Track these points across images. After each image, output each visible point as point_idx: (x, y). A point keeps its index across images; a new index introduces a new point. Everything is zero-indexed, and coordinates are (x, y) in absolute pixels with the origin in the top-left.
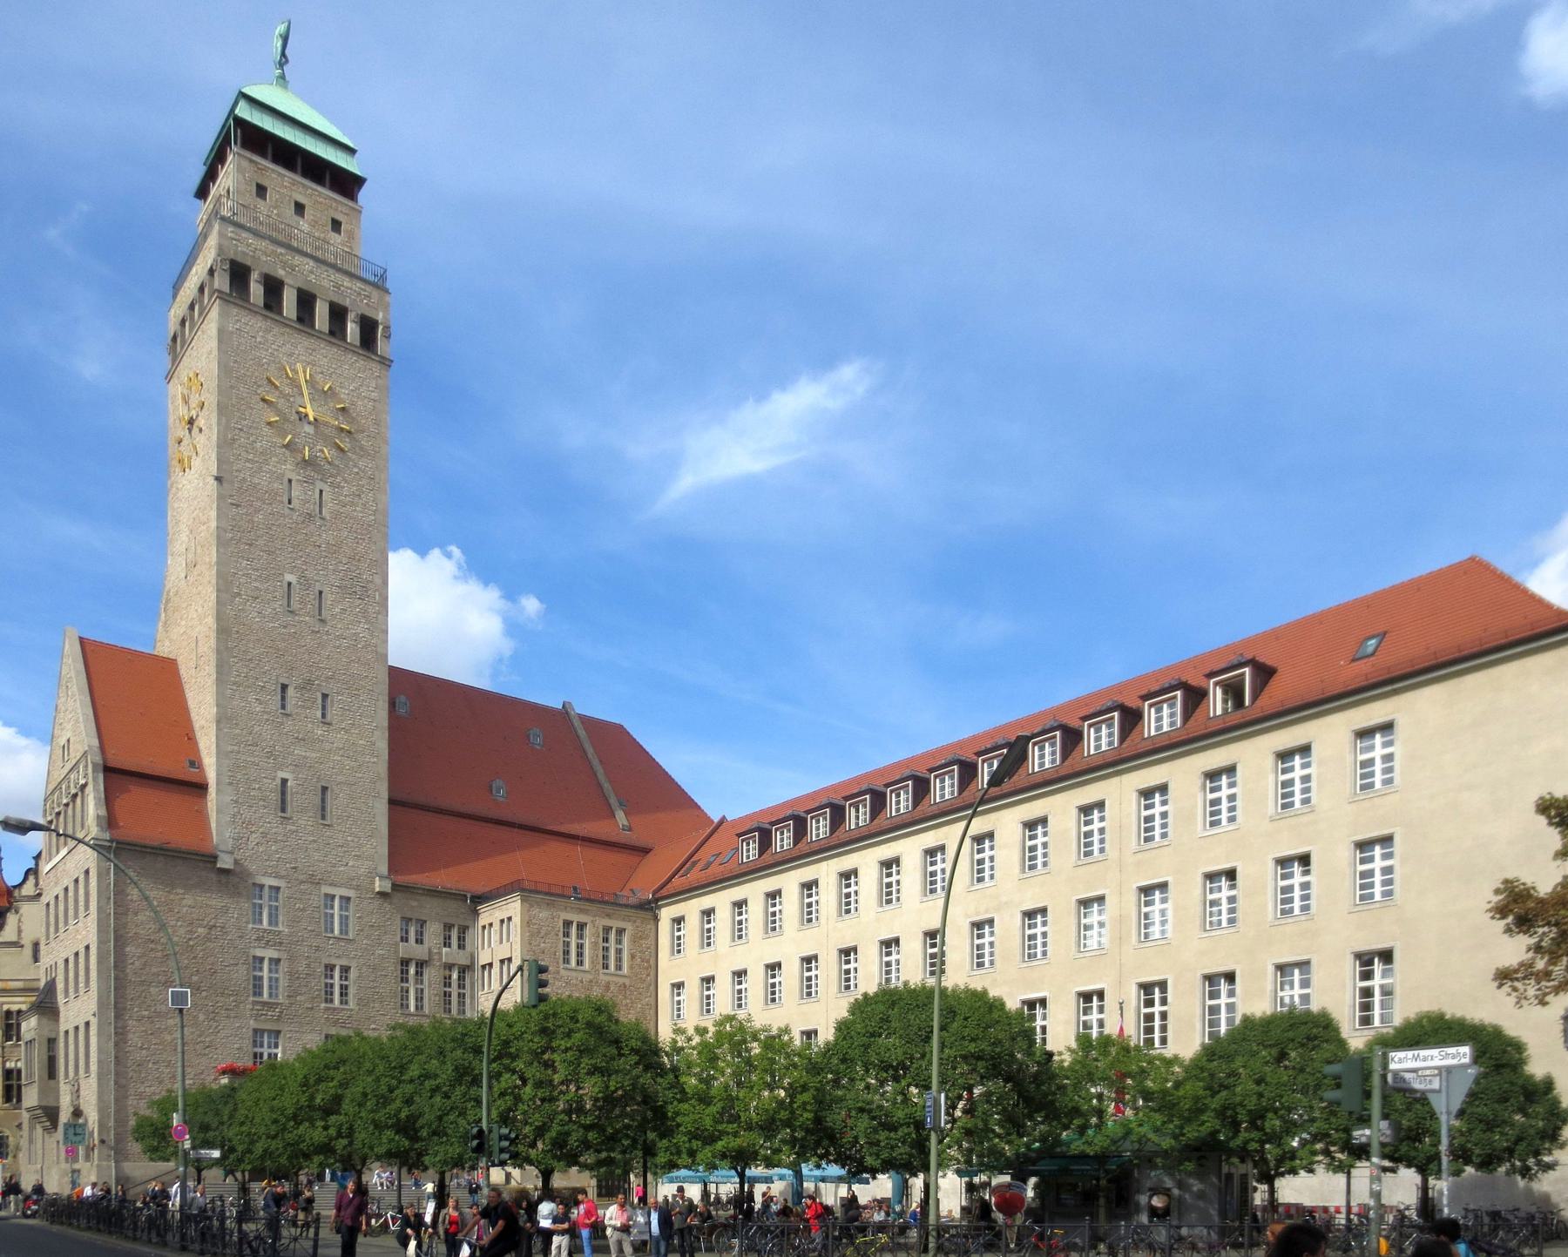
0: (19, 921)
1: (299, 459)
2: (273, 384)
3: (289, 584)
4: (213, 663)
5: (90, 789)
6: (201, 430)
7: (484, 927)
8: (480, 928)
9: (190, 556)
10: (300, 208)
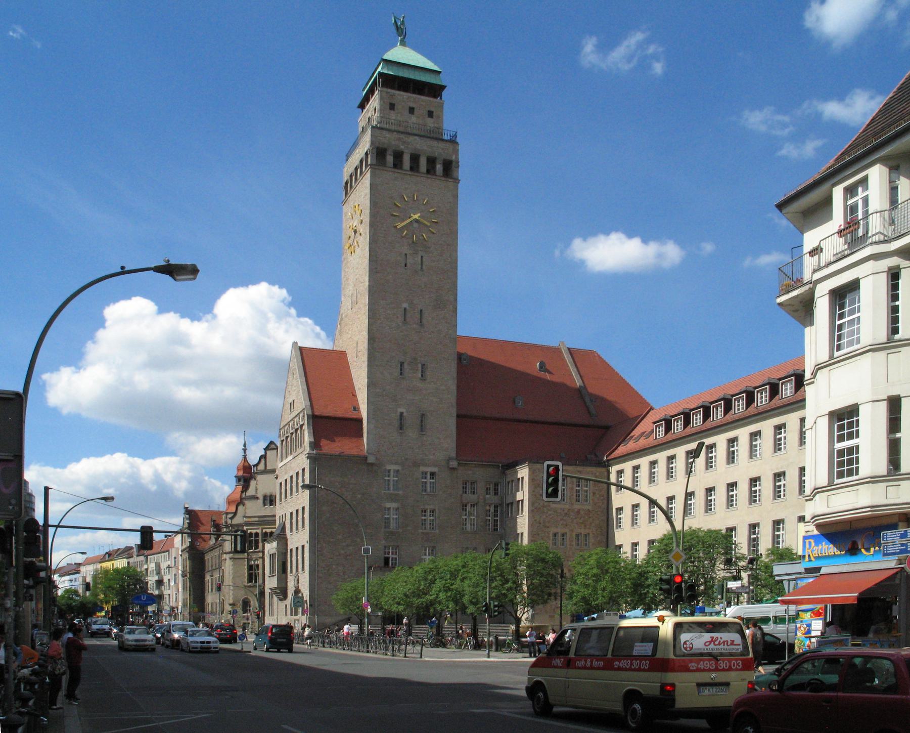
0: (257, 484)
1: (411, 242)
2: (397, 206)
3: (405, 309)
4: (366, 356)
5: (305, 427)
6: (360, 234)
7: (509, 482)
9: (354, 298)
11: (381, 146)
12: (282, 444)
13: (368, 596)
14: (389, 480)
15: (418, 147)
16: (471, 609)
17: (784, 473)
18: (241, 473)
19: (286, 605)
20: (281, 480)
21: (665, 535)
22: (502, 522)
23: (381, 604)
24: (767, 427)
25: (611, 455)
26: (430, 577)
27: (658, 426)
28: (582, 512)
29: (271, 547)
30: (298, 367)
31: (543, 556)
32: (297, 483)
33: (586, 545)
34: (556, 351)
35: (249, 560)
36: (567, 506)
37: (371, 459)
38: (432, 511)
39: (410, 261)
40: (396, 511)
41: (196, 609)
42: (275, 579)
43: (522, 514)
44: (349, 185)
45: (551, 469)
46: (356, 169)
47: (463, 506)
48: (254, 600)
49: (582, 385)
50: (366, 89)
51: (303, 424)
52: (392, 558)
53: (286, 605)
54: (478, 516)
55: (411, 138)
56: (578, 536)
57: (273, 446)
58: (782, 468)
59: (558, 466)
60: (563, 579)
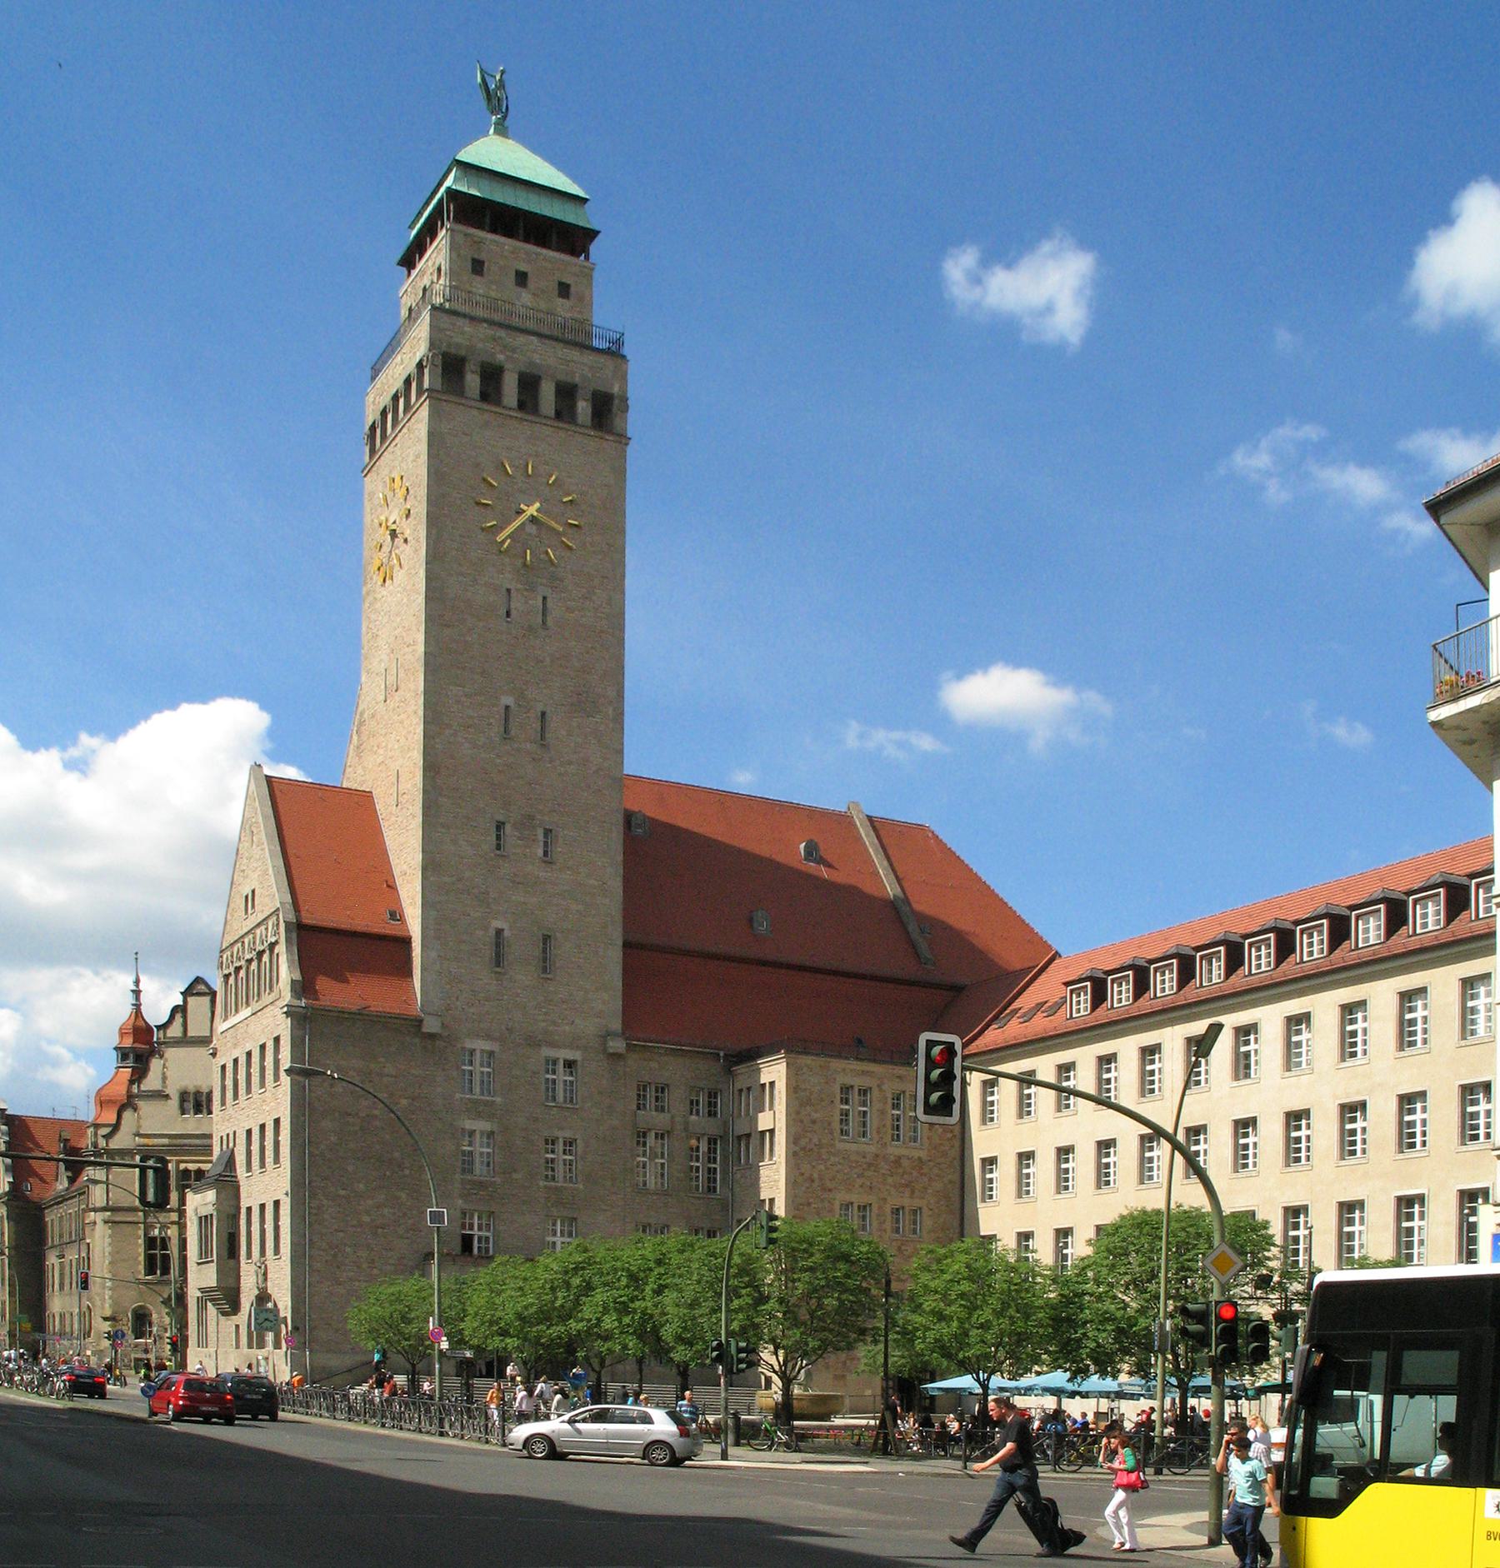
0: (164, 1066)
3: (507, 708)
6: (406, 541)
8: (736, 1092)
9: (391, 679)
10: (522, 278)
11: (453, 351)
12: (226, 983)
13: (440, 1316)
14: (471, 1073)
15: (537, 358)
16: (680, 1354)
17: (1362, 1106)
18: (128, 1042)
19: (237, 1327)
20: (225, 1058)
21: (1123, 1217)
22: (725, 1172)
23: (462, 1334)
24: (1324, 1005)
25: (977, 1042)
26: (576, 1281)
27: (1077, 992)
28: (905, 1163)
29: (201, 1202)
30: (265, 817)
31: (845, 1248)
32: (277, 1062)
33: (914, 1231)
34: (842, 821)
35: (148, 1227)
36: (873, 1149)
37: (431, 1025)
38: (569, 1143)
39: (517, 604)
40: (488, 1138)
41: (28, 1326)
42: (211, 1270)
43: (771, 1159)
44: (378, 431)
45: (936, 1050)
46: (395, 398)
47: (639, 1137)
48: (159, 1313)
49: (901, 895)
50: (418, 226)
51: (277, 942)
52: (480, 1239)
53: (237, 1327)
54: (671, 1159)
55: (522, 339)
56: (895, 1212)
57: (202, 988)
58: (1358, 1093)
59: (953, 1044)
60: (891, 1300)
